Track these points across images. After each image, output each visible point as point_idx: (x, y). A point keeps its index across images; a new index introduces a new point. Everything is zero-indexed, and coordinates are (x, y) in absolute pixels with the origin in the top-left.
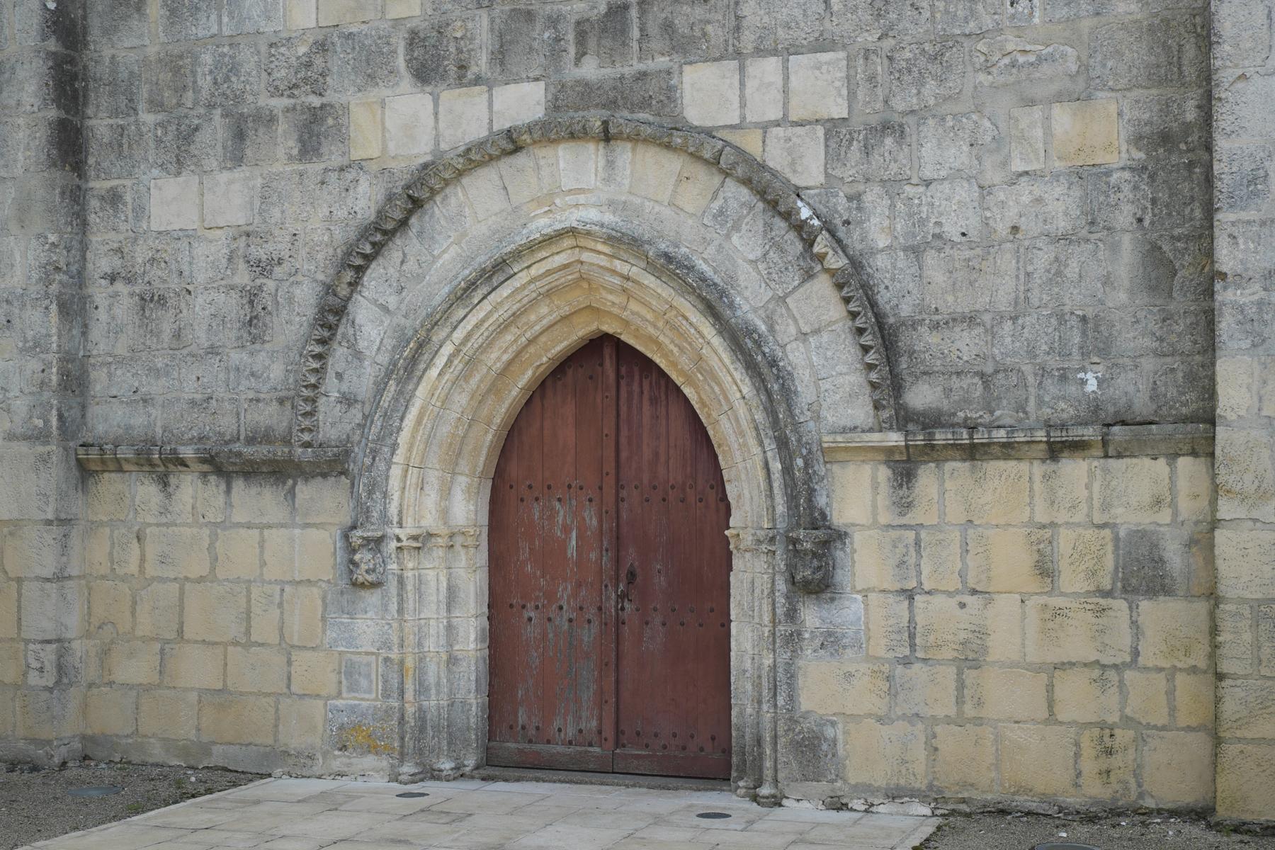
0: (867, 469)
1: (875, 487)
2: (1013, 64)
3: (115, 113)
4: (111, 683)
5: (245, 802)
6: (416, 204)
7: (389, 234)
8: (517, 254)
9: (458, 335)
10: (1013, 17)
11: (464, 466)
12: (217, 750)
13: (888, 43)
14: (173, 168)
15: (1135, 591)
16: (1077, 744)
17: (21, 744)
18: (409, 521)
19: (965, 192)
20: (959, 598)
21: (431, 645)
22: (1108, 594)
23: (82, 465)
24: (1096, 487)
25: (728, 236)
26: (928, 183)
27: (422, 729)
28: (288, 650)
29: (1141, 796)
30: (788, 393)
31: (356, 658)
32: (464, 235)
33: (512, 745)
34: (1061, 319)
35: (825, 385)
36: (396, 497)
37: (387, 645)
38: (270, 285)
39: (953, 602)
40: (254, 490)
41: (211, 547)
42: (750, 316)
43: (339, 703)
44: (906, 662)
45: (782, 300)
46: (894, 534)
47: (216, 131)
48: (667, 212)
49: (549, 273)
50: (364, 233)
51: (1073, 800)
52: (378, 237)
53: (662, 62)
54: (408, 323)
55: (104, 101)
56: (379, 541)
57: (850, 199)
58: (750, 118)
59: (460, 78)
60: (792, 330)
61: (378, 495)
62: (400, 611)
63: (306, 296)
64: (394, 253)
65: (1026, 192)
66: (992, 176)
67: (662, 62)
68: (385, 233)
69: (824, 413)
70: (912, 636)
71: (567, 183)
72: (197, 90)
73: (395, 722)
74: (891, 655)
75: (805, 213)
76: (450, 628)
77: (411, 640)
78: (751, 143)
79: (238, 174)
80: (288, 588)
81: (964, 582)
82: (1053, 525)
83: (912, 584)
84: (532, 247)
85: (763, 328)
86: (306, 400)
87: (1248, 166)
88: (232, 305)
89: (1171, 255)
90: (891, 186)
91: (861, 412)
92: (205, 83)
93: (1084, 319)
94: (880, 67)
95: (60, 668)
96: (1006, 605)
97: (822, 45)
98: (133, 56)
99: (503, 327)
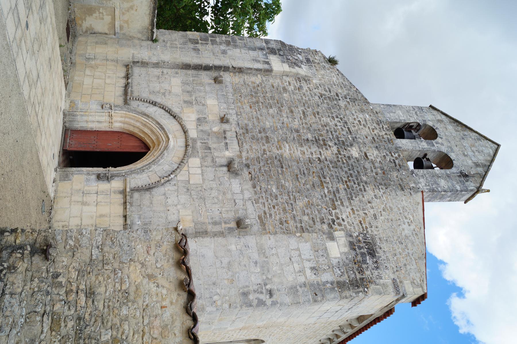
3: (192, 74)
4: (86, 67)
6: (175, 117)
7: (169, 113)
8: (165, 131)
9: (150, 123)
11: (126, 125)
12: (72, 83)
13: (203, 190)
14: (182, 82)
16: (65, 221)
18: (115, 114)
19: (176, 202)
23: (128, 65)
25: (168, 165)
26: (178, 196)
27: (73, 116)
30: (138, 173)
34: (151, 218)
35: (139, 180)
36: (120, 112)
44: (83, 193)
45: (156, 173)
47: (189, 88)
49: (160, 135)
52: (169, 111)
53: (200, 155)
55: (194, 73)
56: (111, 109)
57: (175, 184)
58: (190, 168)
59: (198, 125)
60: (150, 175)
61: (120, 109)
62: (97, 112)
63: (159, 100)
64: (166, 114)
66: (179, 207)
69: (133, 180)
70: (88, 194)
71: (178, 140)
73: (75, 110)
77: (92, 114)
78: (186, 168)
79: (181, 92)
82: (110, 217)
85: (150, 170)
91: (133, 185)
92: (198, 88)
94: (200, 189)
95: (89, 59)
96: (94, 209)
97: (204, 180)
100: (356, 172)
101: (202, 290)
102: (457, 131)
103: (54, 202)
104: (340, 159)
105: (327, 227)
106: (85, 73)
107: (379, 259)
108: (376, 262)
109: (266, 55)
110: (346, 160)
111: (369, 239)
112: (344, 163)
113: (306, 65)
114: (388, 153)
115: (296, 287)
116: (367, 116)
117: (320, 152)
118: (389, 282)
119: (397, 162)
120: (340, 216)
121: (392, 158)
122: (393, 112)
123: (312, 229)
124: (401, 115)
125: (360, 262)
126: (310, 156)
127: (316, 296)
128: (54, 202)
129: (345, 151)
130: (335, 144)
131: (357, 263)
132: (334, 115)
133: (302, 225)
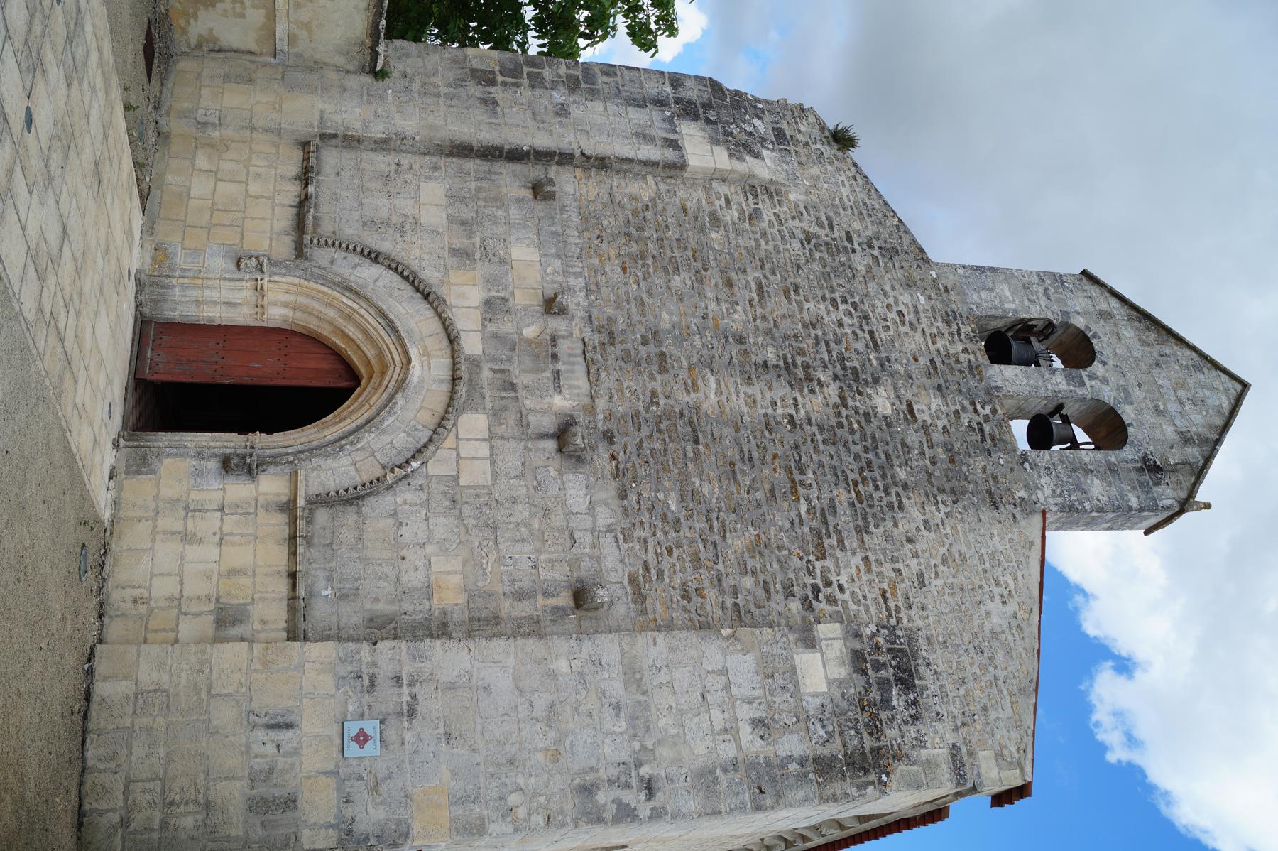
0: (287, 491)
1: (279, 495)
2: (482, 558)
5: (131, 194)
6: (426, 297)
7: (412, 283)
8: (399, 338)
9: (362, 312)
10: (504, 557)
11: (299, 315)
12: (158, 193)
13: (494, 503)
14: (449, 194)
15: (218, 613)
16: (139, 587)
17: (168, 104)
18: (271, 285)
19: (422, 537)
20: (219, 532)
21: (207, 293)
22: (217, 600)
24: (272, 595)
25: (405, 432)
26: (427, 520)
27: (163, 287)
28: (209, 228)
29: (111, 617)
31: (202, 257)
32: (411, 317)
33: (152, 333)
34: (358, 579)
35: (330, 473)
37: (208, 271)
38: (391, 231)
39: (216, 529)
40: (290, 218)
41: (263, 197)
42: (365, 440)
43: (179, 249)
44: (186, 508)
45: (373, 455)
46: (253, 502)
47: (466, 213)
48: (418, 406)
49: (391, 353)
50: (413, 273)
51: (109, 585)
52: (411, 278)
53: (489, 406)
54: (369, 290)
56: (262, 271)
57: (421, 486)
59: (485, 319)
60: (357, 459)
65: (421, 563)
66: (430, 549)
67: (489, 406)
68: (413, 281)
70: (199, 511)
72: (484, 207)
73: (168, 273)
74: (190, 500)
75: (415, 465)
76: (215, 303)
77: (210, 283)
78: (450, 442)
79: (445, 221)
80: (239, 229)
81: (226, 535)
82: (254, 575)
83: (227, 511)
84: (403, 345)
85: (359, 446)
86: (334, 242)
87: (428, 654)
88: (383, 214)
89: (388, 627)
90: (427, 504)
91: (315, 488)
92: (488, 211)
93: (358, 589)
94: (484, 499)
95: (205, 124)
96: (214, 553)
97: (495, 474)
98: (502, 182)
99: (366, 333)
100: (883, 456)
101: (482, 779)
102: (1144, 343)
103: (111, 534)
104: (844, 420)
105: (801, 607)
106: (193, 164)
107: (922, 694)
108: (915, 703)
109: (670, 120)
110: (859, 423)
111: (902, 640)
112: (852, 432)
113: (773, 150)
114: (966, 403)
115: (712, 772)
116: (921, 298)
117: (795, 399)
118: (943, 753)
119: (987, 428)
120: (834, 578)
121: (976, 419)
122: (988, 289)
123: (763, 611)
124: (1007, 298)
125: (875, 705)
126: (770, 411)
127: (761, 796)
128: (111, 534)
129: (858, 397)
130: (836, 377)
131: (867, 708)
132: (837, 295)
133: (738, 601)
